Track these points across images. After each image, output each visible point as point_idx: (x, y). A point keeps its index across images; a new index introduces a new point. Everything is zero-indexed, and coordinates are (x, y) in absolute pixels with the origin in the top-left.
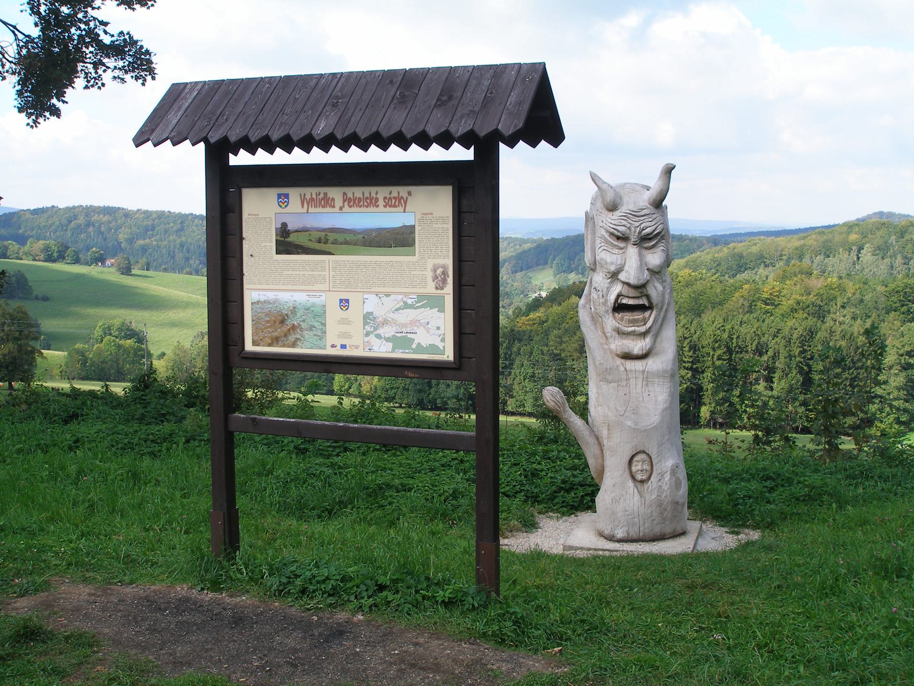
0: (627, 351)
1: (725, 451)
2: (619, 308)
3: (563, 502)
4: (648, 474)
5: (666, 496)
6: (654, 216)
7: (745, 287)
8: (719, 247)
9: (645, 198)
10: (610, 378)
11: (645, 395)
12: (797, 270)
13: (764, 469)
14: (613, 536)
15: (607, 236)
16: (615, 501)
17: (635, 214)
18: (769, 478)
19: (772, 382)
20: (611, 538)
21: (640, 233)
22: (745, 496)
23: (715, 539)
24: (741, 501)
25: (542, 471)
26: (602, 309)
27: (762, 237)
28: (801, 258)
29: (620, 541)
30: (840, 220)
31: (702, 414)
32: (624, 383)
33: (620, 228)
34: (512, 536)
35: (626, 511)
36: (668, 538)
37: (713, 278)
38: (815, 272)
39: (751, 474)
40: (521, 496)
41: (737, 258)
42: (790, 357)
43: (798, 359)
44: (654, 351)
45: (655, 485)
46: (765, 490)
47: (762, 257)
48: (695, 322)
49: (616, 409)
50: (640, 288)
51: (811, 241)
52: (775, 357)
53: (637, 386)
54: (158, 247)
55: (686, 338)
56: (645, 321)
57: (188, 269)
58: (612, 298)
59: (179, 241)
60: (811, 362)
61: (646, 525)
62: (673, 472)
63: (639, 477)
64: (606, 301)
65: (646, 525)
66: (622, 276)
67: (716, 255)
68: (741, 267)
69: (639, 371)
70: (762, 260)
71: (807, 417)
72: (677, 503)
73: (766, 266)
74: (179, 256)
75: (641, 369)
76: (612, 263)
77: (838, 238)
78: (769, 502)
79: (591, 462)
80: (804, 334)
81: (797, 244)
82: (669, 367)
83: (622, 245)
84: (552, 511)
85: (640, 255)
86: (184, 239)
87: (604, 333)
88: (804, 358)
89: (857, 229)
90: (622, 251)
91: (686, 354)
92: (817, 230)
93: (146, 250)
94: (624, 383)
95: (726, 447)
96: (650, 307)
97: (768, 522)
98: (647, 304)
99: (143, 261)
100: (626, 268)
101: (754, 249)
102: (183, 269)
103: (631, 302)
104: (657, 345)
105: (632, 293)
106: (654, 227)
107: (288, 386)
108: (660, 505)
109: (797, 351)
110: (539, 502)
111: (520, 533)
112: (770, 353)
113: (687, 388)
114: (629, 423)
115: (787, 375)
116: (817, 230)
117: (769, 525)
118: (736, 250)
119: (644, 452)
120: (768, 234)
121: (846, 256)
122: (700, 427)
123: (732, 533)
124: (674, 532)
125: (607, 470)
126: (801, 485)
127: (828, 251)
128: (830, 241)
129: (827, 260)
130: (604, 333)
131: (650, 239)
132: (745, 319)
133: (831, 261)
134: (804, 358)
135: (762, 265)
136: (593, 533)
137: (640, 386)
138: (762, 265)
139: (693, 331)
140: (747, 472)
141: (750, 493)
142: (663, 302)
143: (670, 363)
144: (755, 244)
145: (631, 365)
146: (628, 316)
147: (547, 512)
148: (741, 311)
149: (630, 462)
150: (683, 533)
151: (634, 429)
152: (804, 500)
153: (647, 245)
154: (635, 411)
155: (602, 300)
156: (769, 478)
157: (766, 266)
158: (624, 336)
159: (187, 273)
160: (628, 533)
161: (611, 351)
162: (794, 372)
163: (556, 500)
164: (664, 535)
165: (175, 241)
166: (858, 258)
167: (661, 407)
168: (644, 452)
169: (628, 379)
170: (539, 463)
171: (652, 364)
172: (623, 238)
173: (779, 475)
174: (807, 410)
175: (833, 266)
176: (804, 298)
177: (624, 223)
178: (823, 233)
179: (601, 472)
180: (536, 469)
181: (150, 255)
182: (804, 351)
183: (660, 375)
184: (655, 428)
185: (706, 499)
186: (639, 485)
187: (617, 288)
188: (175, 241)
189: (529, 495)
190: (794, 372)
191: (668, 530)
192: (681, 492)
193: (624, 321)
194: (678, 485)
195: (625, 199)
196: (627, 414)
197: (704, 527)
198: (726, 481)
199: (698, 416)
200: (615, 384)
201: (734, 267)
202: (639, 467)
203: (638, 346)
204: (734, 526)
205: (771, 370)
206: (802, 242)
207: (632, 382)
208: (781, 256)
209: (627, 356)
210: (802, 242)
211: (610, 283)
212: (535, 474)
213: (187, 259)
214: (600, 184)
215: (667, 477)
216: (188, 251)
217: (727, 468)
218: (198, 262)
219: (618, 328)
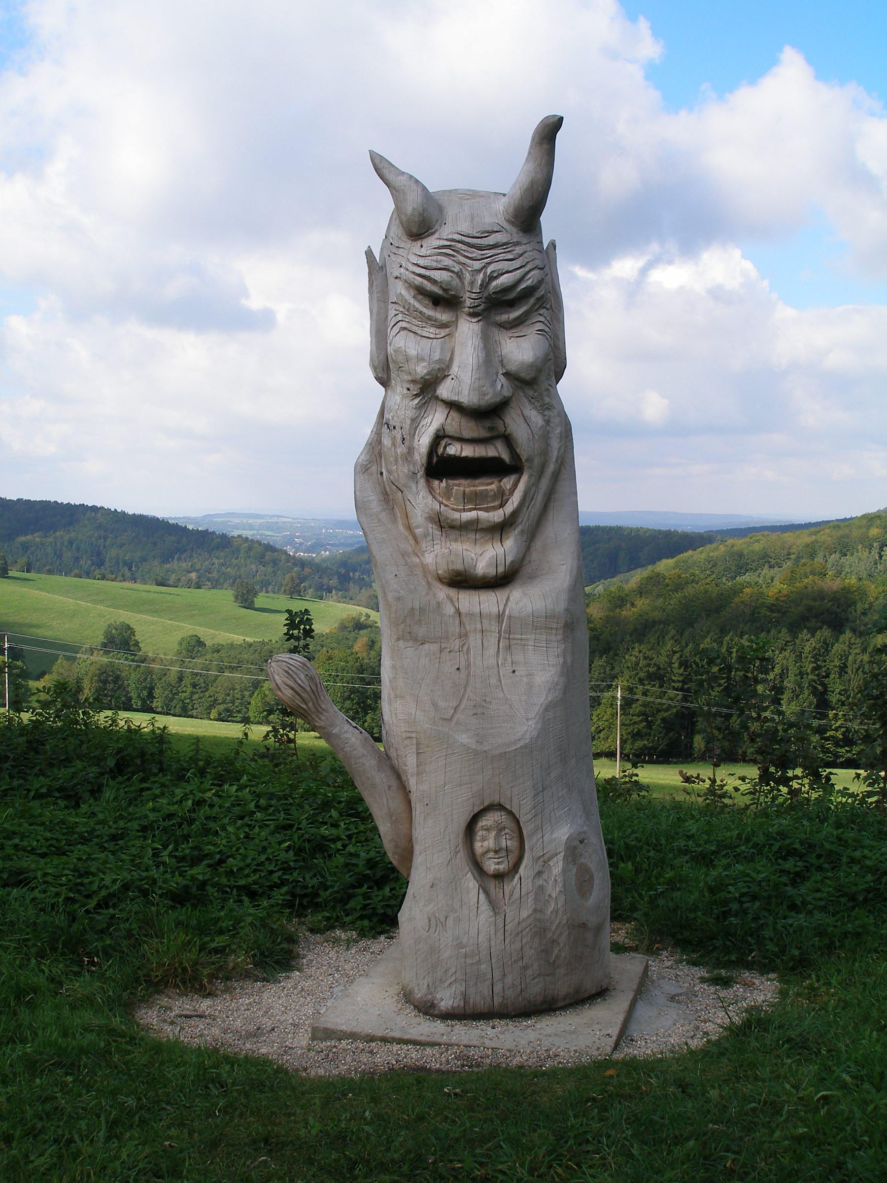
0: (459, 567)
1: (714, 795)
2: (439, 467)
3: (365, 907)
4: (513, 858)
5: (556, 911)
6: (518, 250)
7: (747, 590)
8: (715, 545)
9: (496, 213)
10: (421, 631)
11: (505, 670)
12: (808, 570)
13: (782, 835)
14: (433, 1005)
15: (408, 296)
16: (436, 923)
17: (475, 243)
18: (790, 853)
19: (780, 704)
20: (427, 1009)
21: (484, 285)
22: (743, 895)
23: (675, 1014)
24: (735, 906)
25: (335, 840)
26: (404, 470)
27: (766, 533)
28: (812, 556)
29: (448, 1016)
30: (858, 512)
31: (696, 745)
32: (457, 643)
33: (437, 275)
34: (227, 990)
35: (461, 946)
36: (564, 1008)
37: (707, 581)
38: (830, 573)
39: (755, 845)
40: (280, 895)
41: (736, 557)
42: (801, 674)
43: (811, 677)
44: (527, 570)
45: (527, 885)
46: (785, 879)
47: (766, 555)
48: (687, 633)
49: (435, 705)
50: (488, 415)
51: (824, 537)
52: (783, 675)
53: (484, 653)
54: (42, 544)
55: (675, 652)
56: (502, 498)
57: (76, 571)
58: (424, 441)
59: (66, 538)
60: (826, 681)
61: (509, 980)
62: (573, 852)
63: (491, 866)
64: (411, 450)
65: (509, 980)
66: (445, 391)
67: (711, 554)
68: (741, 568)
69: (490, 615)
70: (766, 559)
71: (822, 747)
72: (583, 926)
73: (771, 567)
74: (68, 555)
75: (494, 610)
76: (420, 359)
77: (856, 533)
78: (793, 907)
79: (384, 827)
80: (818, 646)
81: (807, 540)
82: (562, 606)
83: (443, 316)
84: (343, 926)
85: (486, 338)
86: (73, 534)
87: (409, 528)
88: (818, 675)
89: (879, 522)
90: (443, 332)
91: (675, 671)
92: (831, 524)
93: (27, 548)
94: (457, 643)
95: (715, 792)
96: (514, 468)
97: (792, 958)
98: (505, 456)
99: (22, 561)
100: (455, 369)
101: (757, 547)
102: (71, 571)
103: (468, 451)
104: (534, 556)
105: (470, 429)
106: (518, 274)
107: (194, 712)
108: (540, 930)
109: (809, 667)
110: (317, 907)
111: (248, 984)
112: (777, 670)
113: (677, 712)
114: (464, 738)
115: (797, 696)
116: (831, 524)
117: (792, 966)
118: (735, 548)
119: (500, 807)
120: (773, 529)
121: (866, 554)
122: (693, 761)
123: (717, 981)
124: (577, 991)
125: (417, 848)
126: (856, 868)
127: (844, 548)
128: (847, 536)
129: (843, 559)
130: (409, 528)
131: (512, 304)
132: (746, 629)
133: (848, 560)
134: (818, 675)
135: (767, 566)
136: (394, 990)
137: (492, 651)
138: (767, 566)
139: (683, 644)
140: (748, 840)
141: (755, 888)
142: (545, 453)
143: (564, 597)
144: (758, 541)
145: (468, 601)
146: (461, 486)
147: (331, 928)
148: (741, 619)
149: (470, 829)
150: (601, 993)
151: (476, 753)
152: (865, 900)
153: (504, 317)
154: (480, 710)
155: (401, 449)
156: (790, 853)
157: (771, 567)
158: (454, 534)
159: (76, 576)
160: (465, 997)
161: (424, 567)
162: (806, 692)
163: (352, 904)
164: (554, 1000)
165: (62, 537)
166: (881, 557)
167: (541, 699)
168: (500, 807)
169: (464, 636)
170: (335, 825)
171: (521, 600)
172: (445, 300)
173: (811, 846)
174: (822, 739)
175: (851, 566)
176: (818, 603)
177: (447, 262)
178: (839, 527)
179: (408, 854)
180: (324, 837)
181: (33, 553)
182: (818, 667)
183: (539, 623)
184: (528, 750)
185: (661, 902)
186: (492, 885)
187: (436, 419)
188: (62, 537)
189: (298, 891)
190: (806, 692)
191: (563, 987)
192: (591, 901)
193: (452, 499)
194: (584, 883)
195: (450, 213)
196: (459, 716)
197: (654, 966)
198: (705, 860)
199: (691, 747)
200: (434, 647)
201: (733, 568)
202: (490, 843)
203: (486, 557)
204: (719, 964)
205: (779, 690)
206: (814, 538)
207: (474, 641)
208: (789, 554)
209: (462, 581)
210: (814, 538)
211: (419, 407)
212: (321, 847)
213: (77, 559)
214: (391, 177)
215: (557, 866)
216: (78, 549)
217: (708, 833)
218: (89, 562)
219: (439, 514)
